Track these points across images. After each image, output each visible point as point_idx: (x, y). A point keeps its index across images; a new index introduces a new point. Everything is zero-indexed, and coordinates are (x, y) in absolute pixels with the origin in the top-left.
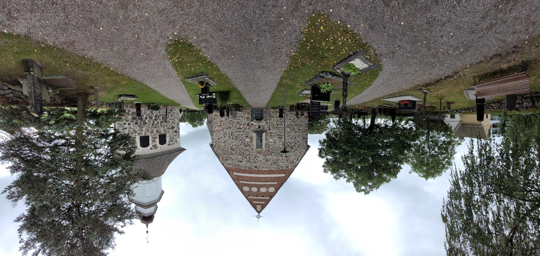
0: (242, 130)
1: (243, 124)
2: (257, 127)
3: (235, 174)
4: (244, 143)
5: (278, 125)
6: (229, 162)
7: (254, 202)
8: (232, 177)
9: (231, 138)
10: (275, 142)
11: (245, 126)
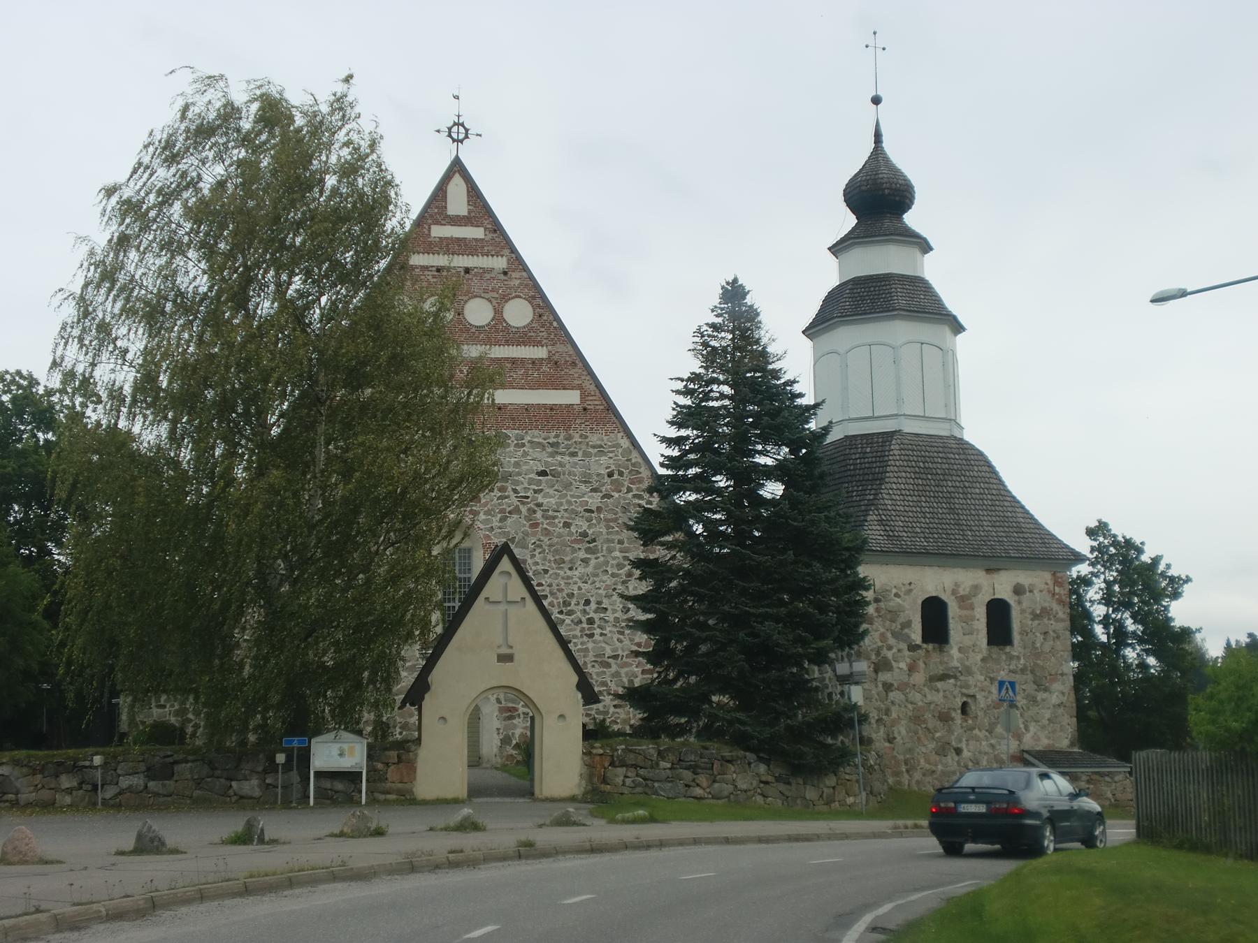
3: (571, 397)
6: (600, 465)
8: (591, 373)
9: (593, 606)
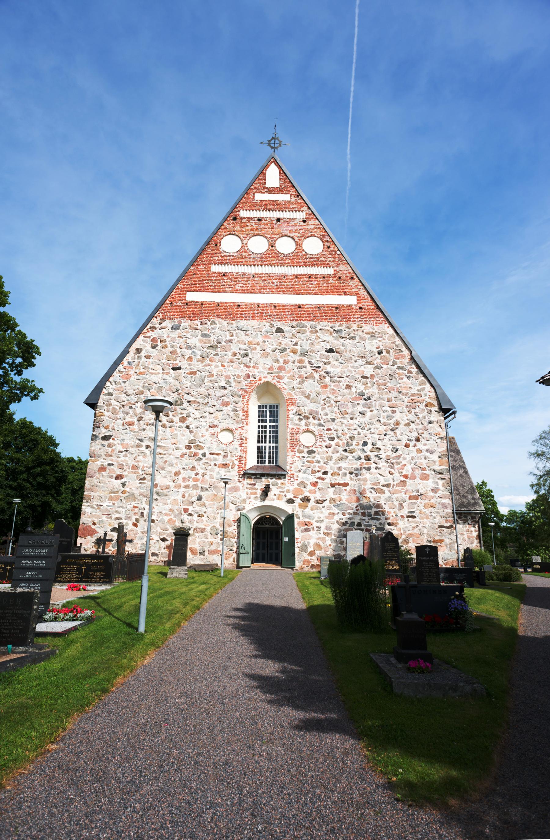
0: (329, 479)
1: (326, 504)
2: (274, 490)
4: (320, 425)
5: (200, 499)
7: (287, 197)
9: (370, 446)
11: (318, 496)
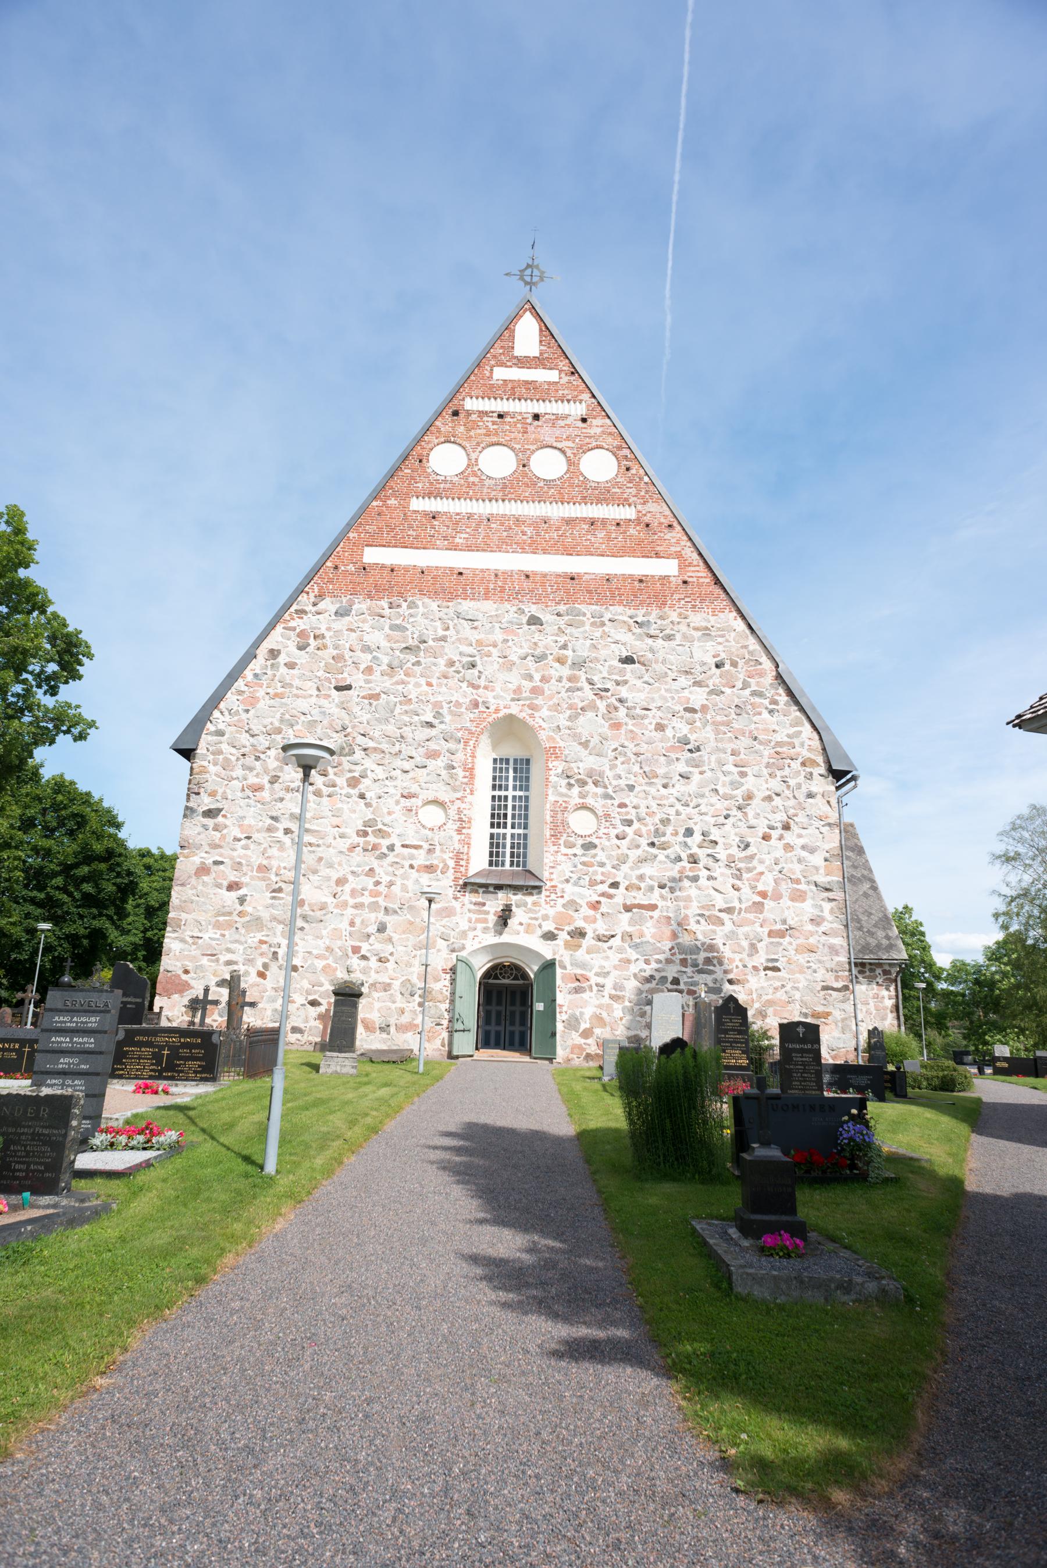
0: (621, 896)
1: (616, 942)
3: (668, 567)
5: (382, 929)
7: (552, 376)
9: (697, 837)
10: (408, 803)
11: (601, 927)
